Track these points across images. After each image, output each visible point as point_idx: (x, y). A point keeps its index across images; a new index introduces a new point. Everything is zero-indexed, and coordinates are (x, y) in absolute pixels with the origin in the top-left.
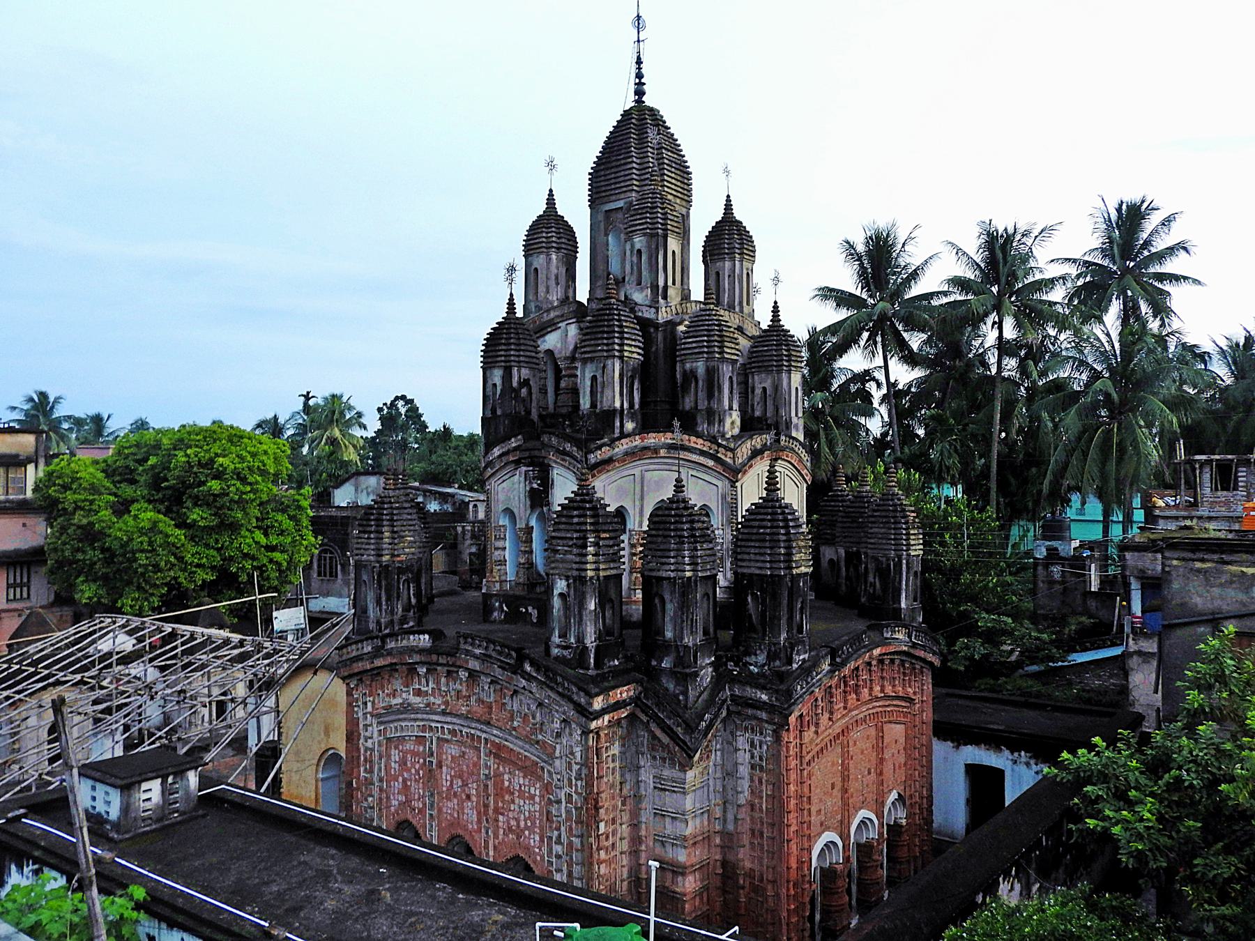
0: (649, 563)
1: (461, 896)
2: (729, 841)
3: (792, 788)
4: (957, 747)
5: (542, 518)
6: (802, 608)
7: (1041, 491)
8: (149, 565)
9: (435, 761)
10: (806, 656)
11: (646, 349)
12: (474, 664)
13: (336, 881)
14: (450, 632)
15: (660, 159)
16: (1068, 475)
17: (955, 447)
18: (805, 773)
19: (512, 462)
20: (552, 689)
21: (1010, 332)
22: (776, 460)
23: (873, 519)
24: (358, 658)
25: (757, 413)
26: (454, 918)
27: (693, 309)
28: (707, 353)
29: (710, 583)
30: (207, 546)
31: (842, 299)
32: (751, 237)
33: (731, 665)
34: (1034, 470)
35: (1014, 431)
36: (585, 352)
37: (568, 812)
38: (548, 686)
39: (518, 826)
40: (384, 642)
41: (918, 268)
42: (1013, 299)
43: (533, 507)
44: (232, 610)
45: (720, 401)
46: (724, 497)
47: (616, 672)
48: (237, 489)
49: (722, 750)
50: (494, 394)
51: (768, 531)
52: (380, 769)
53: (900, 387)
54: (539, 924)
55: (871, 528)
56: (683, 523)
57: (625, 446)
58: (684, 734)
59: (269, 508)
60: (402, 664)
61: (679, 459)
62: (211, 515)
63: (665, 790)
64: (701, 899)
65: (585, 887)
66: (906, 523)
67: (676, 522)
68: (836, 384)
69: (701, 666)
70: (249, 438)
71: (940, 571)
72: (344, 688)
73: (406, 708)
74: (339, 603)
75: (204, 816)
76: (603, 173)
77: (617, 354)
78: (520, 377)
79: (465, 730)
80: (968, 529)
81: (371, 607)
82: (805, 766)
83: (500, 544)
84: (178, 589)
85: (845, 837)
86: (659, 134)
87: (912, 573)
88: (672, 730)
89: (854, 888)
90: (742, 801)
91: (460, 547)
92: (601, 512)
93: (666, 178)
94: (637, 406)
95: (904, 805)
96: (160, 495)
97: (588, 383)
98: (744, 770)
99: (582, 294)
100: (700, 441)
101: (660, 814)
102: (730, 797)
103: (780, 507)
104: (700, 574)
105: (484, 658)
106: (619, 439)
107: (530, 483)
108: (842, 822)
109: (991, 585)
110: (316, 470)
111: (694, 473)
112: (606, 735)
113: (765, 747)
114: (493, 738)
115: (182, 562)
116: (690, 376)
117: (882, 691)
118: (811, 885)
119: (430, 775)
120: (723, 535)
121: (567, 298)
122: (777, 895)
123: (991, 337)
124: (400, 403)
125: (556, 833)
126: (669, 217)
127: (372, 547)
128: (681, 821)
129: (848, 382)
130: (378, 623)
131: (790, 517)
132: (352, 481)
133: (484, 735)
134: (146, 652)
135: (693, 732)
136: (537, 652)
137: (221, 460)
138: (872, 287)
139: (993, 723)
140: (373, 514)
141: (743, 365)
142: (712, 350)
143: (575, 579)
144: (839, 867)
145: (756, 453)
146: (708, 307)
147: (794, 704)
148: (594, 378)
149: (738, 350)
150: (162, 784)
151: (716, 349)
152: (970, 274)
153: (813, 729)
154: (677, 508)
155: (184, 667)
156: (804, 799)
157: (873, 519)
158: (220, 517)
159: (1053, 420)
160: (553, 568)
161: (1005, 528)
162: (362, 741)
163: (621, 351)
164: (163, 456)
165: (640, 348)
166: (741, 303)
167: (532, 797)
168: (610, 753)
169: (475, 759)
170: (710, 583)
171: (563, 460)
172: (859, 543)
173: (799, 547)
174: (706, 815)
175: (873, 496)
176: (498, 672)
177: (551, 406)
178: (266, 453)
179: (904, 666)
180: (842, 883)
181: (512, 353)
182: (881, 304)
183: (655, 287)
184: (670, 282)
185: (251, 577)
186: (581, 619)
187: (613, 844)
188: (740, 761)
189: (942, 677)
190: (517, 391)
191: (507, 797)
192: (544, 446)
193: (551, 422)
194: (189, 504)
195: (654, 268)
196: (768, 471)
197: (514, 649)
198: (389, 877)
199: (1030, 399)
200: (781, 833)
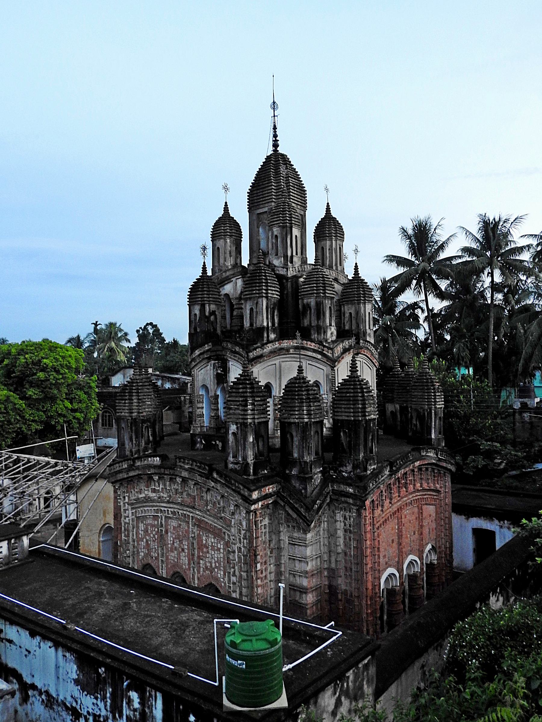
0: (284, 414)
1: (176, 606)
2: (332, 573)
3: (368, 542)
4: (467, 519)
5: (223, 390)
6: (372, 439)
7: (517, 370)
8: (5, 421)
9: (164, 530)
10: (375, 466)
11: (282, 292)
12: (185, 474)
13: (106, 598)
14: (171, 456)
15: (287, 183)
16: (533, 360)
17: (467, 345)
18: (376, 534)
19: (206, 358)
20: (229, 487)
21: (498, 279)
22: (357, 354)
23: (415, 387)
24: (120, 472)
25: (347, 328)
26: (172, 618)
27: (308, 268)
28: (316, 293)
29: (319, 425)
30: (38, 410)
31: (400, 261)
32: (342, 227)
33: (332, 472)
34: (514, 358)
35: (501, 336)
36: (246, 295)
37: (239, 558)
38: (226, 486)
39: (211, 566)
40: (134, 462)
41: (444, 242)
42: (499, 259)
43: (218, 384)
44: (52, 445)
45: (324, 321)
46: (327, 376)
47: (266, 477)
48: (54, 377)
49: (327, 521)
50: (195, 320)
51: (352, 395)
52: (133, 535)
53: (435, 311)
54: (215, 620)
55: (414, 392)
56: (303, 391)
57: (270, 348)
58: (305, 512)
59: (73, 387)
60: (145, 474)
61: (300, 354)
62: (39, 392)
63: (295, 544)
64: (317, 608)
65: (249, 601)
66: (434, 389)
67: (298, 391)
68: (397, 311)
69: (314, 473)
70: (61, 348)
71: (458, 417)
72: (112, 488)
73: (147, 499)
74: (113, 442)
75: (32, 562)
76: (255, 192)
77: (264, 295)
78: (210, 309)
79: (180, 512)
80: (474, 392)
81: (126, 442)
82: (376, 529)
83: (200, 405)
84: (22, 434)
85: (400, 571)
86: (287, 169)
87: (438, 418)
88: (298, 510)
89: (407, 601)
90: (340, 550)
91: (183, 409)
92: (255, 386)
93: (291, 194)
94: (276, 325)
95: (436, 552)
96: (11, 381)
97: (248, 312)
98: (340, 533)
99: (245, 262)
100: (313, 344)
101: (292, 559)
102: (333, 548)
103: (359, 381)
104: (313, 420)
105: (190, 470)
106: (266, 344)
107: (217, 370)
108: (398, 562)
109: (487, 425)
110: (101, 366)
111: (310, 362)
112: (260, 513)
113: (352, 519)
114: (196, 516)
115: (24, 419)
116: (307, 307)
117: (421, 486)
118: (380, 599)
119: (162, 538)
120: (326, 397)
121: (237, 264)
122: (360, 604)
123: (487, 281)
124: (149, 328)
125: (232, 570)
126: (293, 216)
127: (127, 408)
128: (304, 562)
129: (404, 310)
130: (131, 451)
131: (364, 386)
132: (122, 372)
133: (191, 515)
134: (3, 470)
135: (310, 511)
136: (220, 466)
137: (45, 360)
138: (418, 254)
139: (489, 504)
140: (127, 389)
141: (338, 300)
142: (319, 291)
143: (241, 424)
144: (398, 588)
145: (345, 351)
146: (316, 267)
147: (368, 494)
148: (251, 310)
149: (334, 291)
150: (8, 544)
151: (321, 291)
152: (474, 245)
153: (380, 508)
154: (299, 383)
155: (24, 478)
156: (375, 549)
157: (415, 387)
158: (45, 393)
159: (524, 327)
160: (228, 418)
161: (497, 392)
162: (122, 519)
163: (267, 293)
164: (12, 359)
165: (277, 291)
166: (336, 265)
167: (219, 549)
168: (263, 524)
169: (186, 528)
170: (319, 425)
171: (235, 356)
172: (407, 401)
173: (370, 404)
174: (319, 559)
175: (415, 374)
176: (198, 478)
177: (228, 327)
178: (70, 356)
179: (434, 472)
180: (399, 598)
181: (205, 296)
182: (423, 264)
183: (286, 257)
184: (294, 254)
185: (62, 426)
186: (245, 447)
187: (265, 576)
188: (338, 527)
189: (456, 478)
190: (208, 318)
191: (205, 550)
192: (224, 349)
193: (228, 335)
194: (27, 386)
195: (285, 245)
196: (352, 360)
197: (207, 466)
198: (136, 595)
199: (510, 316)
200: (362, 568)
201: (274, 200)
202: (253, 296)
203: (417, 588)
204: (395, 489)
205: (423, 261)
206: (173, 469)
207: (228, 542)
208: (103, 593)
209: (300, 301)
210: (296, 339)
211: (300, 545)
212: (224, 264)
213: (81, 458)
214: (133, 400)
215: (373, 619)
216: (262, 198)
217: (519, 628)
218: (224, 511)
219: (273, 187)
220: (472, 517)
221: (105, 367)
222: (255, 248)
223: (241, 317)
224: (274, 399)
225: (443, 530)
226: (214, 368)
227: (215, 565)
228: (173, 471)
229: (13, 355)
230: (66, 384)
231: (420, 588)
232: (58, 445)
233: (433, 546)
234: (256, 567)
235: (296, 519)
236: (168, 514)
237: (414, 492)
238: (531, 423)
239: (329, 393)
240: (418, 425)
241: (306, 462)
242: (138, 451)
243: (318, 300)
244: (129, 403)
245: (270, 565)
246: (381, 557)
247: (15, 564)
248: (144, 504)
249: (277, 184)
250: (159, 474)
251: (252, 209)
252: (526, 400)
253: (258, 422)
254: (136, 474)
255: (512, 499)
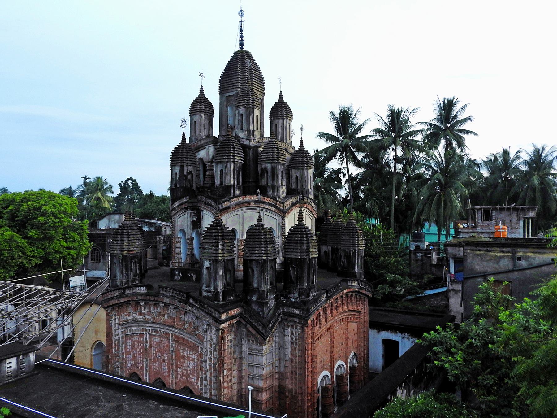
1: (161, 406)
3: (309, 352)
4: (379, 332)
5: (198, 234)
6: (313, 273)
9: (148, 345)
10: (315, 294)
12: (167, 300)
14: (155, 286)
16: (423, 214)
17: (377, 202)
20: (203, 311)
21: (400, 153)
22: (302, 207)
23: (343, 234)
24: (112, 299)
25: (294, 187)
28: (272, 160)
30: (38, 247)
31: (329, 137)
32: (291, 109)
33: (282, 298)
34: (409, 212)
35: (401, 196)
36: (218, 159)
37: (210, 366)
40: (124, 291)
42: (401, 139)
43: (193, 229)
44: (50, 277)
45: (278, 181)
46: (279, 224)
48: (53, 221)
49: (279, 336)
50: (176, 177)
52: (122, 349)
53: (353, 176)
56: (262, 235)
57: (236, 201)
60: (134, 301)
61: (260, 207)
62: (40, 233)
63: (253, 354)
64: (269, 404)
67: (258, 235)
68: (326, 175)
70: (59, 197)
73: (135, 321)
76: (225, 79)
79: (162, 330)
83: (178, 245)
85: (332, 372)
87: (360, 257)
89: (336, 395)
91: (158, 247)
92: (225, 231)
94: (241, 184)
95: (357, 358)
97: (219, 173)
98: (288, 345)
99: (216, 133)
100: (269, 199)
101: (251, 366)
102: (282, 357)
103: (304, 228)
104: (269, 258)
105: (172, 297)
106: (233, 198)
108: (330, 366)
109: (392, 262)
112: (227, 331)
113: (298, 334)
116: (264, 170)
117: (348, 308)
119: (146, 351)
120: (279, 241)
121: (209, 135)
124: (129, 182)
125: (204, 376)
126: (255, 100)
129: (331, 174)
130: (122, 282)
131: (308, 233)
132: (107, 217)
134: (8, 298)
135: (266, 328)
136: (196, 294)
137: (45, 207)
139: (393, 321)
140: (119, 232)
142: (274, 159)
143: (213, 261)
144: (330, 386)
145: (293, 205)
146: (272, 140)
147: (310, 315)
148: (222, 171)
151: (276, 159)
152: (383, 128)
153: (318, 325)
154: (259, 229)
155: (27, 304)
156: (314, 357)
158: (44, 234)
159: (417, 191)
161: (397, 237)
162: (113, 337)
163: (234, 159)
164: (17, 205)
165: (242, 157)
166: (286, 138)
167: (193, 360)
168: (229, 339)
169: (167, 343)
170: (273, 262)
171: (207, 207)
173: (313, 246)
174: (272, 365)
176: (178, 304)
177: (202, 183)
179: (357, 297)
180: (331, 393)
181: (184, 159)
183: (249, 131)
184: (255, 129)
187: (230, 380)
188: (287, 340)
189: (373, 302)
190: (186, 177)
191: (182, 360)
192: (199, 201)
193: (201, 190)
194: (29, 228)
198: (127, 399)
200: (305, 372)
201: (240, 86)
202: (223, 160)
203: (343, 385)
204: (329, 310)
205: (346, 138)
206: (157, 296)
207: (201, 353)
208: (100, 397)
209: (259, 166)
210: (257, 195)
211: (257, 355)
212: (199, 135)
213: (73, 287)
214: (124, 241)
215: (312, 411)
216: (230, 84)
217: (422, 413)
218: (198, 330)
219: (239, 76)
220: (382, 331)
221: (93, 213)
222: (224, 123)
223: (213, 177)
224: (238, 241)
225: (363, 341)
226: (190, 216)
227: (190, 372)
228: (157, 298)
229: (17, 202)
230: (63, 226)
231: (345, 385)
232: (54, 277)
233: (355, 353)
234: (223, 372)
235: (255, 335)
236: (152, 332)
237: (342, 313)
238: (422, 261)
239: (280, 237)
240: (345, 262)
241: (263, 291)
242: (128, 282)
243: (273, 165)
244: (121, 243)
245: (234, 371)
246: (318, 363)
247: (23, 376)
248: (132, 325)
249: (243, 74)
250: (145, 300)
251: (223, 92)
252: (418, 244)
253: (227, 260)
254: (125, 300)
255: (408, 317)
